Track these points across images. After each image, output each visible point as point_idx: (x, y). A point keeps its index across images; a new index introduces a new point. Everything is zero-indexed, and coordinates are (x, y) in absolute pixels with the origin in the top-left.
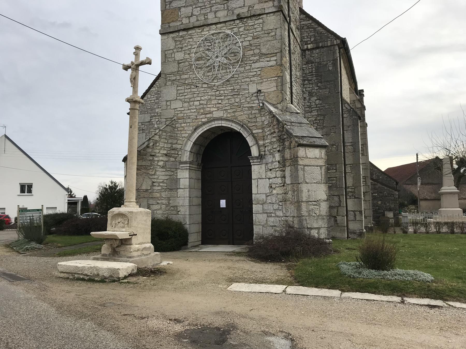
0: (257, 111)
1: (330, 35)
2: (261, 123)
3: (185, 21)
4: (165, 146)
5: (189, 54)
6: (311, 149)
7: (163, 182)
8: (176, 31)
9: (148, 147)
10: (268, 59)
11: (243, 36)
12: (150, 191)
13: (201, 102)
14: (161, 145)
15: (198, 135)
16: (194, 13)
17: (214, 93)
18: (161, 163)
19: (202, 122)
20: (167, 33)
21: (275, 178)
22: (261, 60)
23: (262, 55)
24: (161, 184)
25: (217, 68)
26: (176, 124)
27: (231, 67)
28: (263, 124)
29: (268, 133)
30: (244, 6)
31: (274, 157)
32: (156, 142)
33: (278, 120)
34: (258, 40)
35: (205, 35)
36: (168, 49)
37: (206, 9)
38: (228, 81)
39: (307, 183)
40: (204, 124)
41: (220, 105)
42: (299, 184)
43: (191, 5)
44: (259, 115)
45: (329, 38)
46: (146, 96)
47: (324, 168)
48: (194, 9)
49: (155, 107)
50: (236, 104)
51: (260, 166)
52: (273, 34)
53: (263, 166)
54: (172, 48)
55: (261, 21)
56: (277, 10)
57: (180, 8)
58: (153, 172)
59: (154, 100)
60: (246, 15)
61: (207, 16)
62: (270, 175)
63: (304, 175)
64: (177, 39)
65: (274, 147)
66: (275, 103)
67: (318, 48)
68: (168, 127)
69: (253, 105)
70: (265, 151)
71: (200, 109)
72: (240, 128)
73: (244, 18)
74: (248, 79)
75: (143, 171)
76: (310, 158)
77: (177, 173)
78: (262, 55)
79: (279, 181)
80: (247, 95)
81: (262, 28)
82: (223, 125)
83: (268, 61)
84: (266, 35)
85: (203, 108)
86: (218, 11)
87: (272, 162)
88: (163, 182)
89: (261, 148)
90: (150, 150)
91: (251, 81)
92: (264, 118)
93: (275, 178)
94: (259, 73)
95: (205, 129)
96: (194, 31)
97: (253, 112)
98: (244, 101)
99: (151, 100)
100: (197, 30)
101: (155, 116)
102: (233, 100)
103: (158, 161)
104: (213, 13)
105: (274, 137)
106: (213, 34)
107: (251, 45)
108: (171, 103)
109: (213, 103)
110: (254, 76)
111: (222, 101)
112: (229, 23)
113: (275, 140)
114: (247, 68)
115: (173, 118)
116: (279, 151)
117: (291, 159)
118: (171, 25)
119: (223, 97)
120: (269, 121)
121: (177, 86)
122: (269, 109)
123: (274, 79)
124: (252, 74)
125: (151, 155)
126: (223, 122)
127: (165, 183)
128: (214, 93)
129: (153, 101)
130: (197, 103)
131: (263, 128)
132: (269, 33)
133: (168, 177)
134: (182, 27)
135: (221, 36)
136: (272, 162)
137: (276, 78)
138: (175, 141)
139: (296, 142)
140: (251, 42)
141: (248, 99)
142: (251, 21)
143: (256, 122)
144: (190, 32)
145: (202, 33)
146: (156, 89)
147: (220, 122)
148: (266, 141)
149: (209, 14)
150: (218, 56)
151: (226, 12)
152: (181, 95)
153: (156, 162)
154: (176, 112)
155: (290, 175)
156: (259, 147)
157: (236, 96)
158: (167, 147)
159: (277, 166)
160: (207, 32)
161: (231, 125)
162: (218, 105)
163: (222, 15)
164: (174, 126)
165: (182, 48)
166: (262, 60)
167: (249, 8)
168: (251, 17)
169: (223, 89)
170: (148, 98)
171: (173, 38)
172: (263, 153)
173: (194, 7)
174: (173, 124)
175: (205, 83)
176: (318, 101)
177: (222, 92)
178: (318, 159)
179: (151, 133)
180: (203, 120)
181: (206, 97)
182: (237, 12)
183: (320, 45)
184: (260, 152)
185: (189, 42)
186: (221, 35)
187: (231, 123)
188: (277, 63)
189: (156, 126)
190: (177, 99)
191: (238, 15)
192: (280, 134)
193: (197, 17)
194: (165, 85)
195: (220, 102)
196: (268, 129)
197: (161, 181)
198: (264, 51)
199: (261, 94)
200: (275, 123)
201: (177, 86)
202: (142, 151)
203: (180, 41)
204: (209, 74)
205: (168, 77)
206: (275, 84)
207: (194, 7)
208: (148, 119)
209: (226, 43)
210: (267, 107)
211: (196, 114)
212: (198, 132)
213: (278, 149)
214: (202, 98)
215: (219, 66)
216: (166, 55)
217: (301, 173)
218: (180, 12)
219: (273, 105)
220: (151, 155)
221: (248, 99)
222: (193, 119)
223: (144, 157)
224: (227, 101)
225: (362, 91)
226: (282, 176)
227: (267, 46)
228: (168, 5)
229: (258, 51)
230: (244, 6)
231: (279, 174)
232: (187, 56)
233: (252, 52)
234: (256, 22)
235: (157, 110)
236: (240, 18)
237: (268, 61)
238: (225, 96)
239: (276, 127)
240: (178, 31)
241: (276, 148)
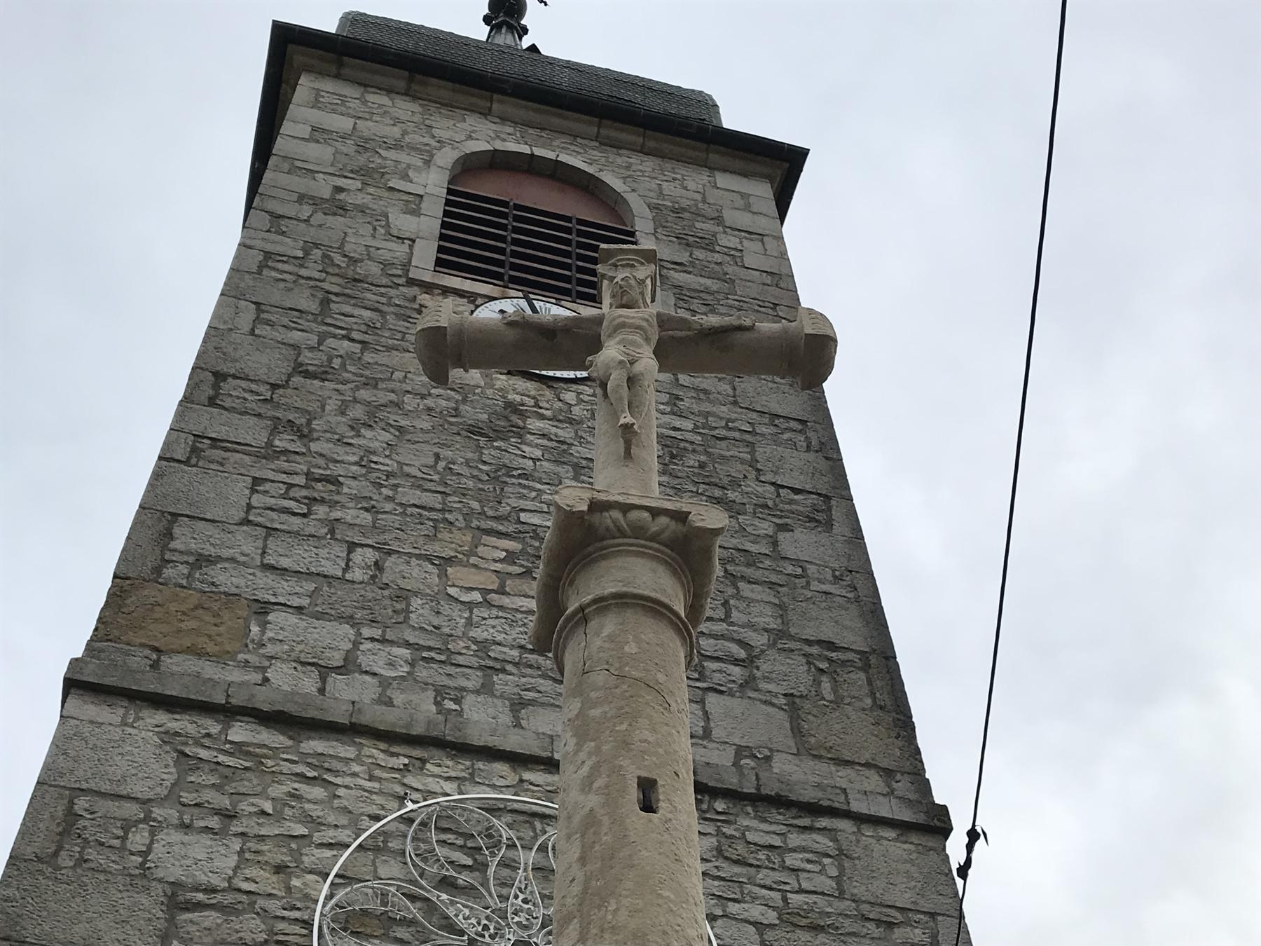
5: (279, 869)
36: (106, 787)
37: (452, 670)
43: (350, 620)
48: (368, 645)
54: (139, 788)
57: (262, 609)
61: (457, 701)
64: (203, 754)
81: (838, 879)
86: (532, 702)
96: (348, 751)
100: (374, 752)
132: (890, 925)
134: (263, 700)
142: (754, 823)
145: (410, 780)
165: (229, 816)
171: (168, 737)
207: (366, 632)
216: (71, 816)
218: (264, 625)
232: (266, 881)
234: (795, 839)
240: (228, 712)
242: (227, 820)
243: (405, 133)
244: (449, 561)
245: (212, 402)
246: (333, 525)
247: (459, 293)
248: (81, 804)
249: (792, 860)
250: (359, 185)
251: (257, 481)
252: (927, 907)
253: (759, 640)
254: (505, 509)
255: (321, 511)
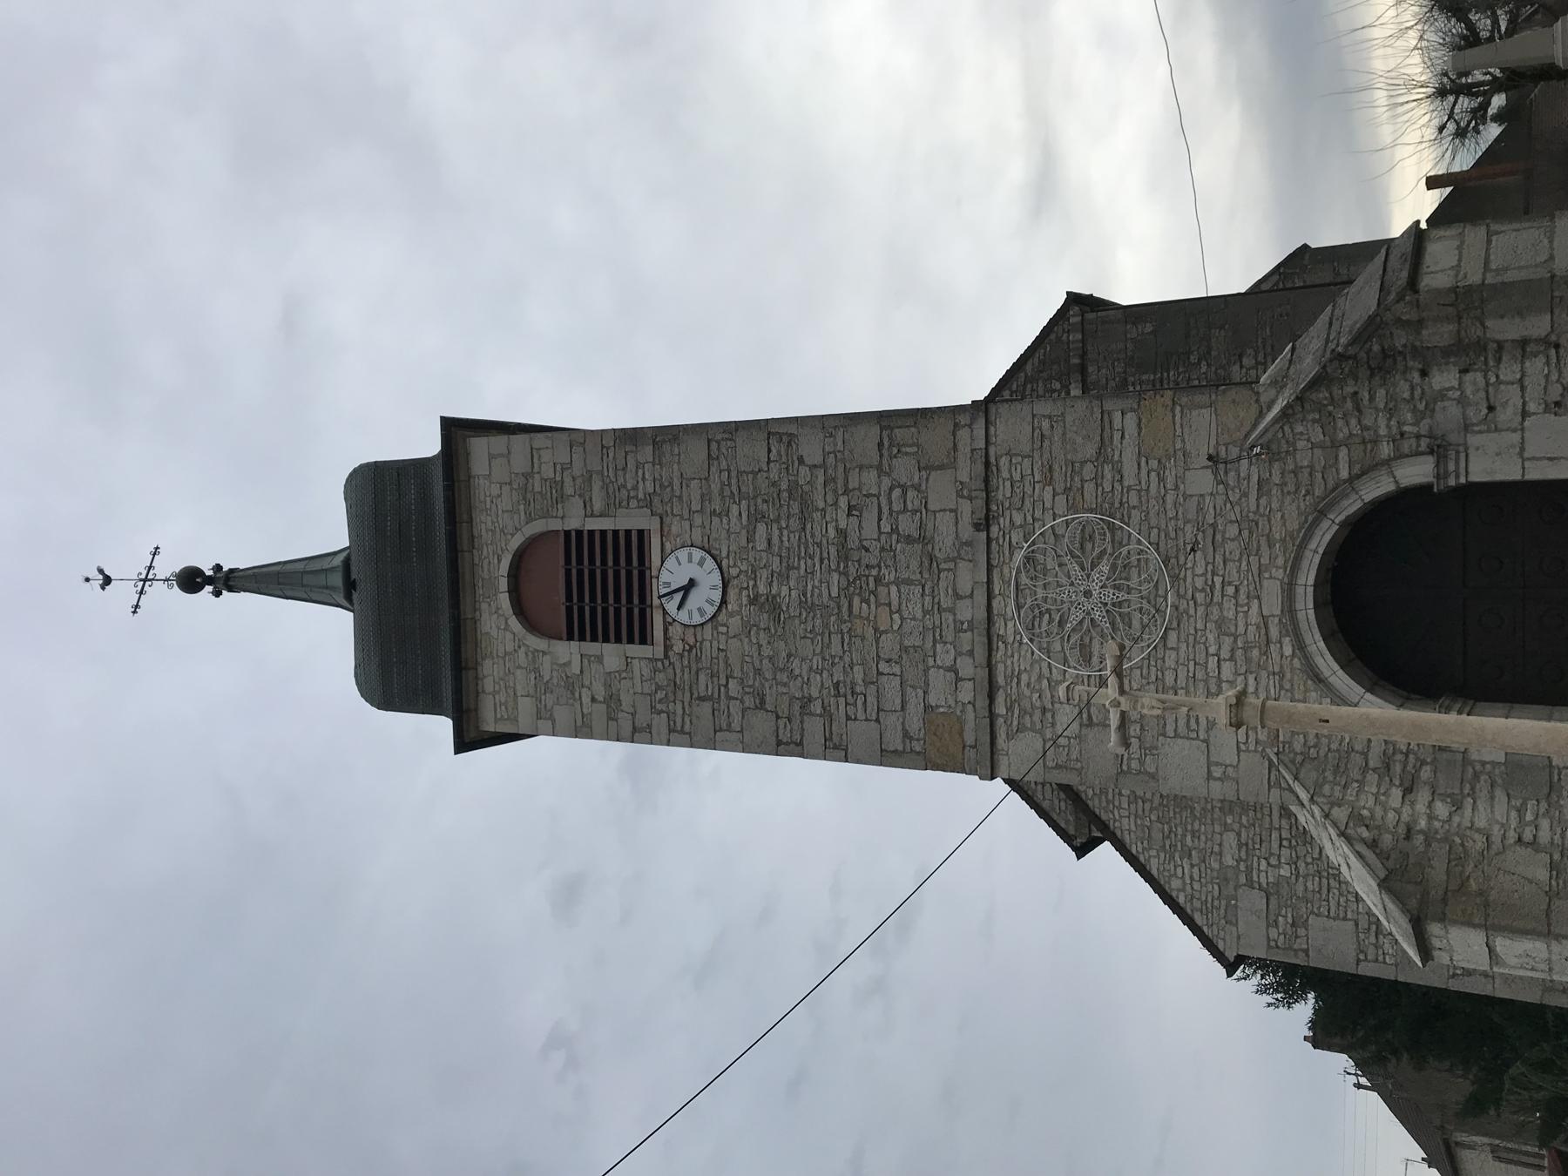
0: (1276, 465)
1: (1053, 336)
2: (1318, 452)
3: (966, 694)
4: (1374, 790)
6: (1428, 259)
7: (1521, 812)
8: (992, 725)
9: (1373, 844)
10: (1117, 436)
11: (1038, 514)
12: (1556, 857)
13: (1225, 654)
14: (1371, 803)
15: (1341, 673)
16: (948, 663)
17: (1201, 610)
18: (1442, 809)
19: (1293, 655)
20: (992, 753)
21: (1523, 389)
22: (1116, 458)
23: (1102, 456)
24: (1529, 817)
25: (1123, 596)
26: (1292, 751)
27: (1124, 550)
28: (1322, 446)
29: (1353, 422)
30: (954, 511)
31: (1442, 395)
32: (1356, 817)
33: (1314, 384)
34: (1056, 467)
35: (1016, 632)
38: (1166, 561)
39: (1552, 258)
40: (1300, 645)
41: (1243, 590)
42: (1553, 277)
43: (926, 671)
44: (1290, 460)
45: (1059, 339)
46: (1174, 894)
47: (1494, 227)
49: (1216, 865)
50: (1245, 533)
51: (1471, 451)
52: (1045, 424)
53: (1473, 440)
54: (1039, 745)
55: (1004, 461)
56: (982, 414)
57: (928, 708)
58: (1476, 836)
59: (1192, 866)
60: (980, 503)
62: (1510, 410)
63: (1520, 268)
64: (1015, 723)
65: (1406, 395)
66: (1254, 409)
67: (1083, 369)
68: (1301, 776)
69: (1255, 478)
70: (1418, 437)
71: (1248, 660)
72: (1325, 524)
73: (988, 510)
74: (1170, 499)
75: (1469, 869)
76: (1460, 260)
77: (1483, 763)
78: (1102, 456)
79: (1536, 366)
80: (1220, 500)
81: (1024, 457)
82: (1311, 581)
83: (1123, 437)
84: (1047, 443)
85: (1246, 649)
86: (954, 590)
87: (1462, 401)
88: (1521, 812)
89: (1406, 451)
90: (1387, 839)
91: (1177, 488)
92: (1301, 444)
93: (1523, 389)
94: (1154, 464)
95: (1322, 644)
96: (1001, 667)
97: (1276, 479)
98: (1237, 509)
99: (1192, 878)
101: (1249, 870)
102: (1230, 546)
103: (1431, 817)
104: (960, 604)
105: (1372, 399)
106: (1019, 607)
107: (1067, 490)
108: (1217, 764)
109: (1231, 615)
110: (1161, 479)
111: (1230, 584)
112: (994, 555)
113: (1381, 393)
114: (1134, 500)
115: (1270, 761)
116: (1424, 373)
117: (1460, 318)
118: (969, 739)
119: (1218, 580)
120: (1314, 421)
121: (1164, 735)
122: (1275, 421)
123: (1178, 418)
124: (1154, 485)
125: (1408, 837)
126: (1301, 581)
127: (1524, 804)
128: (1201, 610)
129: (1196, 870)
130: (1227, 669)
131: (1335, 445)
133: (1500, 794)
134: (982, 702)
135: (1028, 581)
136: (1462, 401)
137: (1178, 409)
138: (1358, 759)
139: (1400, 298)
140: (1060, 487)
141: (1234, 496)
143: (1311, 467)
144: (1001, 680)
146: (1153, 853)
147: (1300, 590)
148: (1383, 431)
149: (959, 617)
150: (1086, 592)
151: (961, 564)
152: (1193, 725)
153: (1437, 824)
154: (1252, 748)
155: (1517, 320)
156: (1400, 456)
157: (1219, 537)
158: (1379, 786)
159: (1479, 376)
160: (1010, 624)
161: (1316, 551)
162: (1242, 597)
163: (968, 576)
164: (1299, 758)
165: (1044, 710)
166: (1117, 453)
167: (962, 497)
168: (987, 490)
169: (1189, 580)
170: (1183, 890)
171: (1009, 737)
172: (1424, 443)
173: (931, 661)
174: (1293, 762)
175: (1164, 638)
176: (1245, 361)
177: (1199, 583)
178: (1462, 243)
179: (1310, 896)
180: (1288, 651)
181: (1211, 637)
182: (967, 532)
183: (1076, 361)
184: (1422, 454)
185: (1028, 685)
186: (1024, 580)
187: (1308, 554)
188: (1132, 410)
189: (1285, 871)
190: (1206, 741)
191: (977, 527)
192: (1363, 373)
193: (961, 654)
194: (1153, 776)
195: (1230, 590)
196: (1340, 423)
197: (1514, 814)
198: (1090, 450)
199: (1223, 454)
200: (1323, 394)
201: (1164, 735)
202: (1390, 864)
203: (1023, 713)
204: (1136, 624)
205: (1129, 766)
206: (1195, 413)
208: (1256, 900)
209: (1051, 564)
210: (1266, 430)
211: (1264, 674)
212: (1326, 673)
213: (1416, 376)
214: (1212, 650)
215: (1115, 587)
217: (1511, 276)
219: (1261, 415)
220: (1408, 837)
221: (1234, 496)
222: (1281, 688)
223: (1412, 860)
224: (1230, 565)
225: (1081, 851)
226: (1518, 353)
227: (1079, 440)
228: (914, 743)
229: (1089, 467)
230: (954, 511)
231: (1509, 371)
233: (1089, 487)
234: (1005, 474)
235: (1229, 861)
236: (985, 523)
237: (1123, 437)
238: (1214, 574)
239: (1337, 392)
240: (992, 716)
241: (1412, 389)
242: (337, 580)
243: (519, 667)
244: (876, 630)
245: (801, 744)
246: (866, 683)
247: (666, 631)
248: (1050, 764)
249: (1017, 477)
250: (584, 690)
251: (848, 718)
252: (1029, 418)
253: (886, 482)
254: (832, 604)
255: (858, 689)
